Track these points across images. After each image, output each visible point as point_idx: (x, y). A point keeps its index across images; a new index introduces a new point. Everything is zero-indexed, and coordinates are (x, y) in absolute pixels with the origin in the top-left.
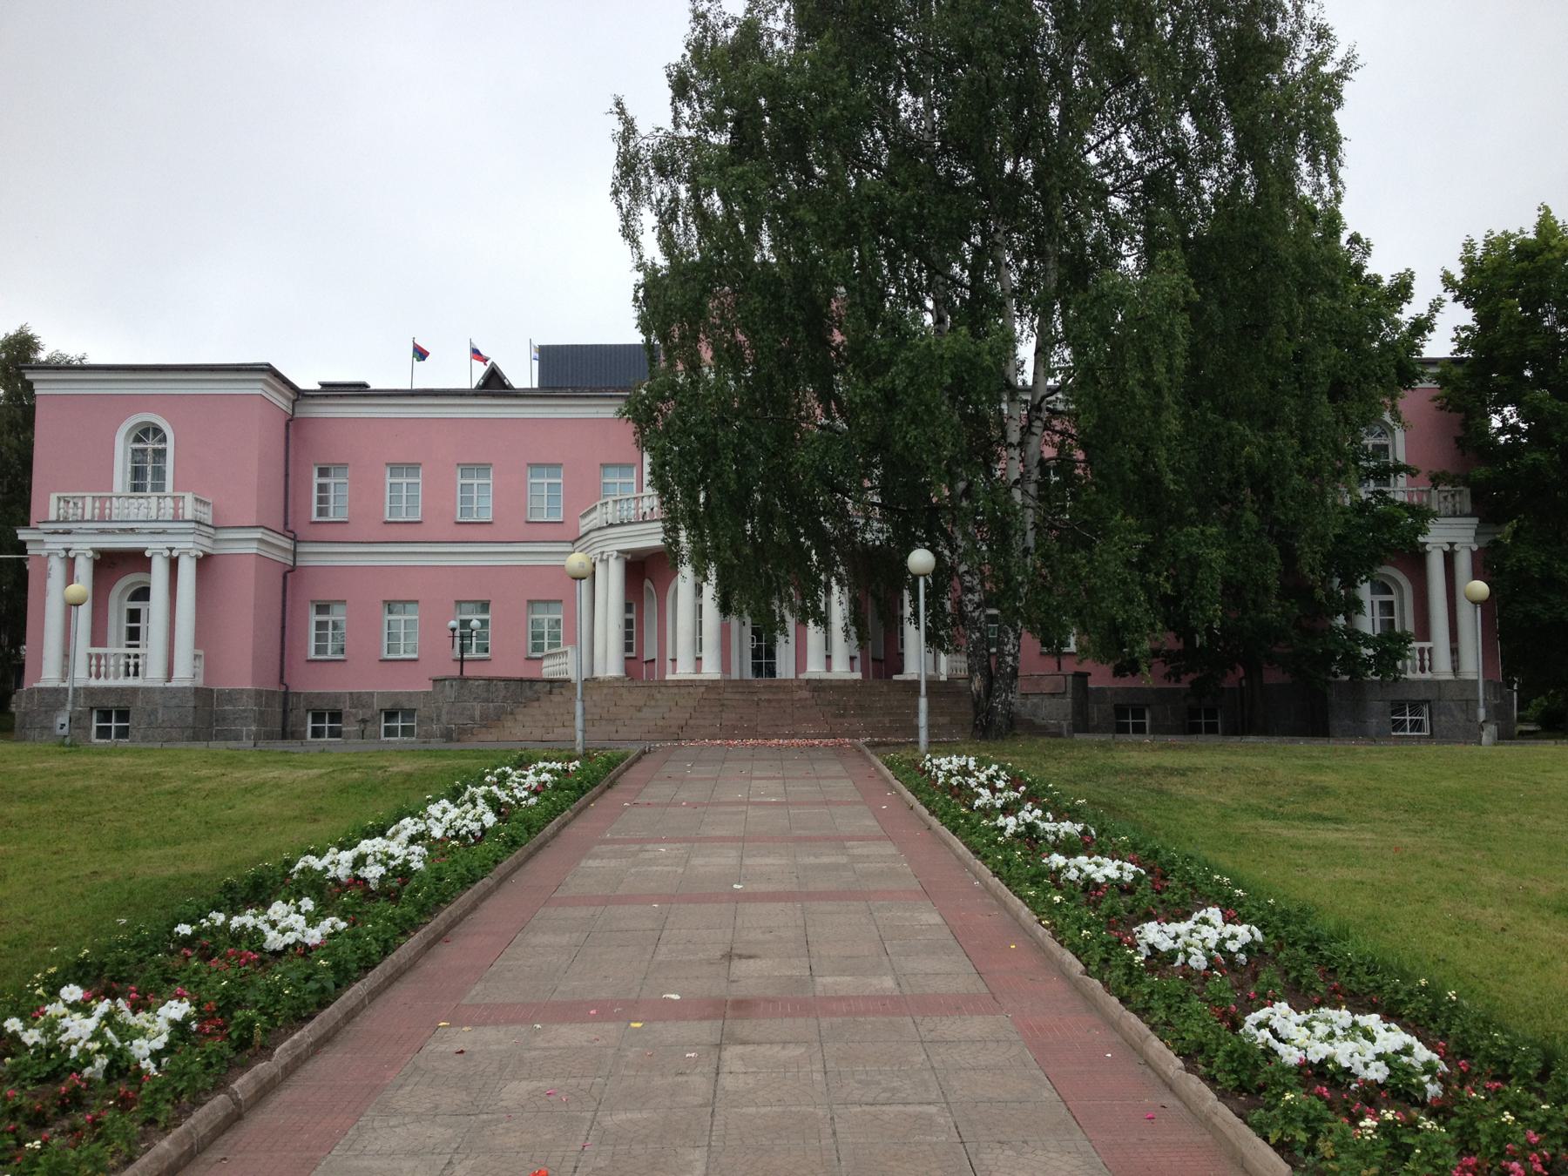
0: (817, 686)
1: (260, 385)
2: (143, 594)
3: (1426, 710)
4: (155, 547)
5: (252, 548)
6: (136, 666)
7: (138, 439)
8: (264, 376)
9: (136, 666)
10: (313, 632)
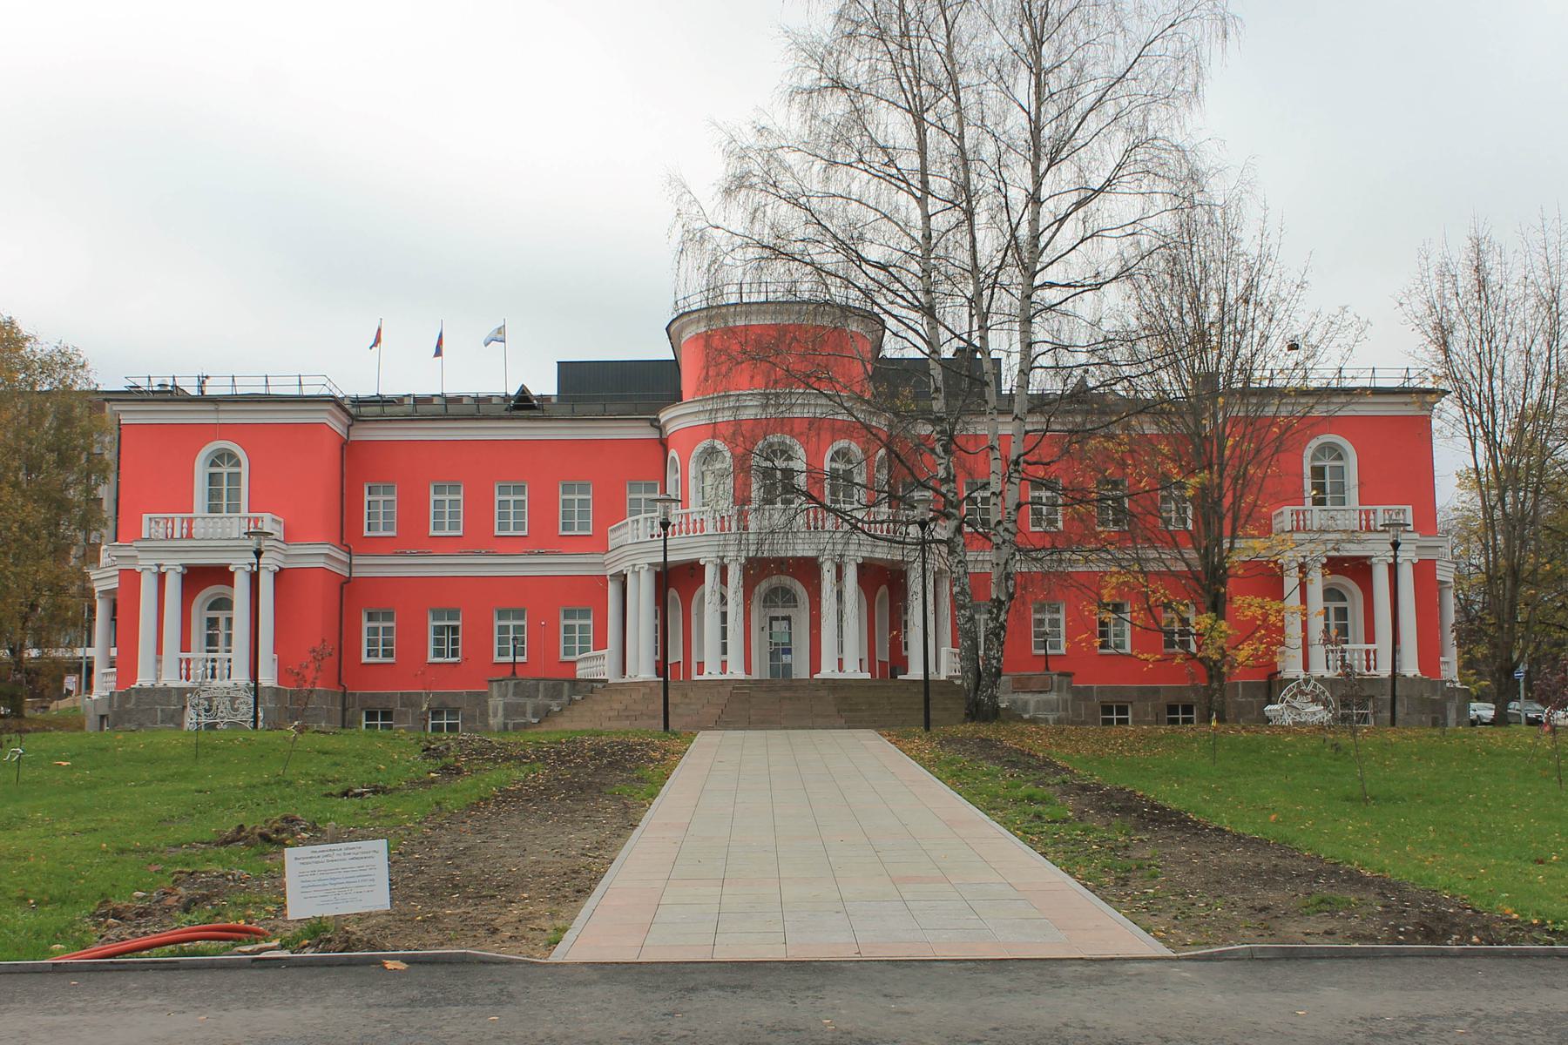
0: (833, 685)
1: (326, 415)
2: (224, 604)
3: (1371, 704)
4: (240, 565)
5: (319, 563)
6: (213, 669)
7: (213, 464)
8: (329, 407)
9: (213, 669)
10: (431, 636)
